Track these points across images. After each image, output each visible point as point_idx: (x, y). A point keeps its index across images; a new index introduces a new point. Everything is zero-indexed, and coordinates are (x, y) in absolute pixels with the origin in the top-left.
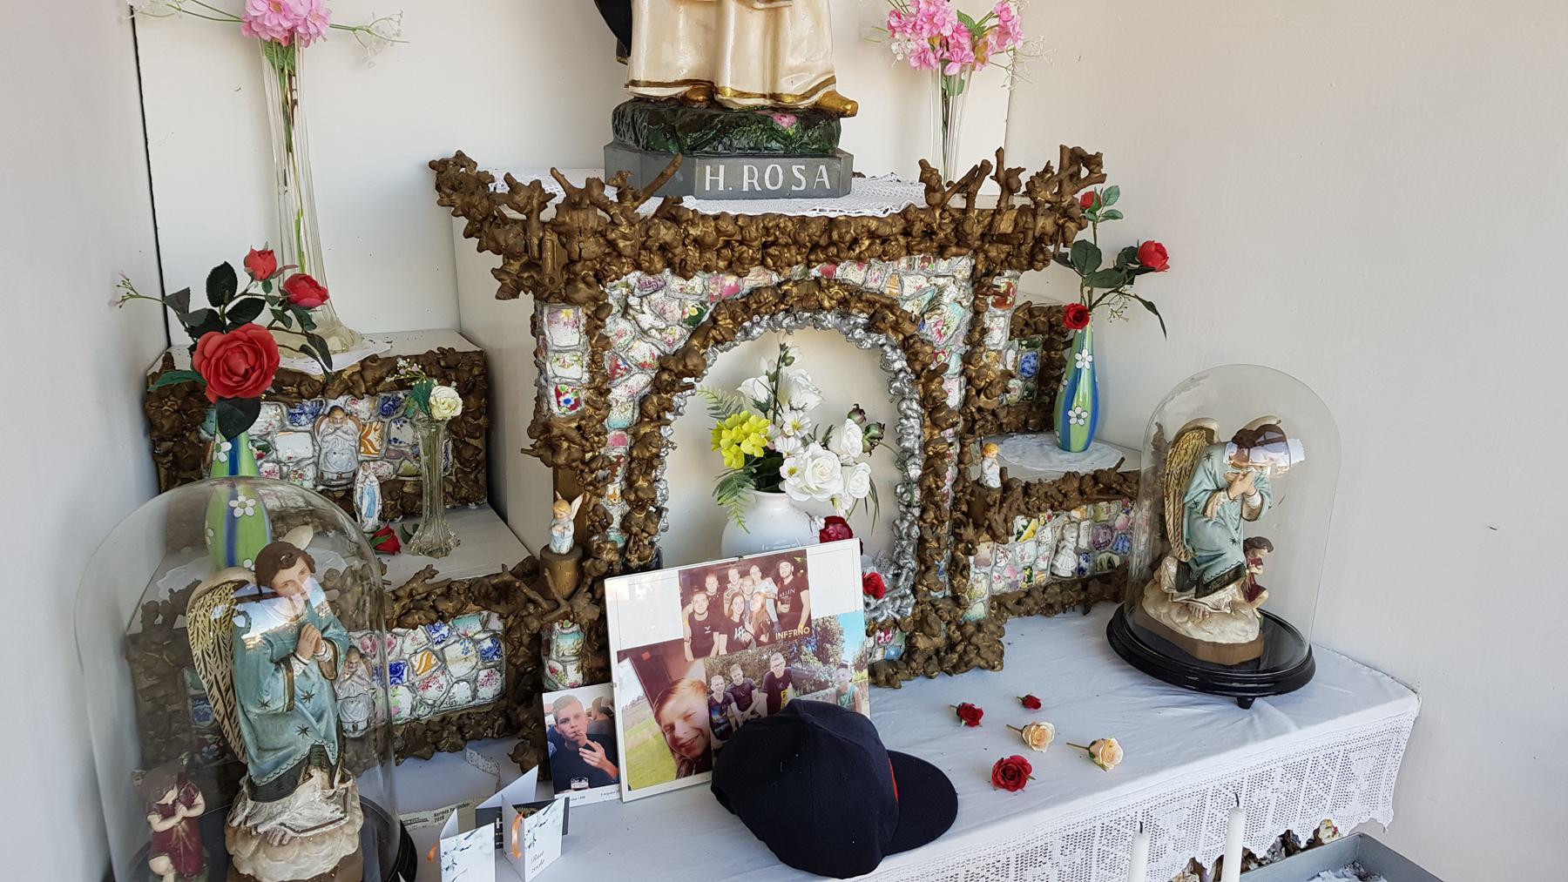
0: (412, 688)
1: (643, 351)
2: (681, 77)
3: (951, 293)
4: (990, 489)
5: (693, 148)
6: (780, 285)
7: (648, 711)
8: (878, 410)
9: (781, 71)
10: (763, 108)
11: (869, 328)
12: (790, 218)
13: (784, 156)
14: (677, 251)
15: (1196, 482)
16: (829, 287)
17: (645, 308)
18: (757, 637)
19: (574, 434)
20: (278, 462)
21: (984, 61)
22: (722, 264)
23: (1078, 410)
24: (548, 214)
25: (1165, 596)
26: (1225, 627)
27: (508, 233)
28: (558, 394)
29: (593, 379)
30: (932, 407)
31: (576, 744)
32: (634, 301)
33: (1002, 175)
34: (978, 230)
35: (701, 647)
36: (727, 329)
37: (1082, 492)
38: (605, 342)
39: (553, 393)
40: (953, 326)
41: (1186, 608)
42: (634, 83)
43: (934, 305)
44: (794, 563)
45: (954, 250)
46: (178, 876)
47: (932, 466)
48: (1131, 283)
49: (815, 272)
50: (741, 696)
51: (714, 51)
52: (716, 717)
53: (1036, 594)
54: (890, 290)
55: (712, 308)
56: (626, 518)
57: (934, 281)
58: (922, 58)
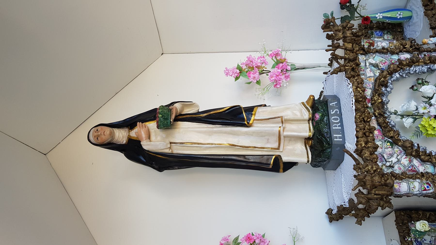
1: (405, 161)
2: (304, 148)
3: (371, 61)
5: (329, 144)
6: (376, 116)
8: (411, 81)
9: (302, 118)
10: (312, 123)
11: (386, 86)
12: (356, 114)
13: (329, 116)
14: (371, 150)
16: (375, 100)
21: (285, 59)
22: (371, 135)
23: (397, 15)
24: (365, 191)
27: (373, 205)
28: (425, 190)
29: (419, 178)
30: (412, 63)
32: (388, 164)
33: (334, 49)
34: (351, 54)
36: (394, 133)
38: (403, 173)
39: (425, 192)
40: (382, 59)
42: (308, 162)
43: (376, 66)
45: (357, 61)
49: (369, 105)
51: (295, 138)
55: (386, 138)
57: (367, 67)
58: (287, 77)
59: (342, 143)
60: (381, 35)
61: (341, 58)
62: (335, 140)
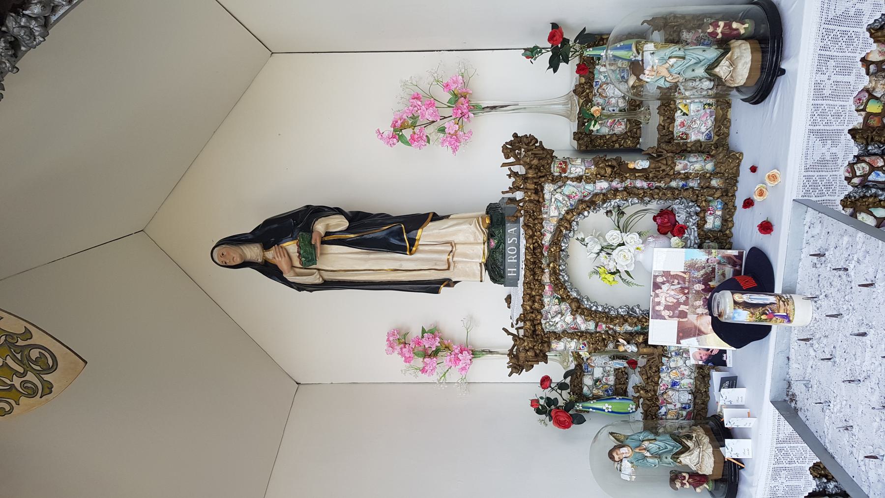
1: (569, 318)
18: (685, 294)
30: (605, 197)
35: (683, 314)
38: (564, 331)
46: (879, 204)
47: (630, 192)
54: (554, 222)
56: (630, 325)
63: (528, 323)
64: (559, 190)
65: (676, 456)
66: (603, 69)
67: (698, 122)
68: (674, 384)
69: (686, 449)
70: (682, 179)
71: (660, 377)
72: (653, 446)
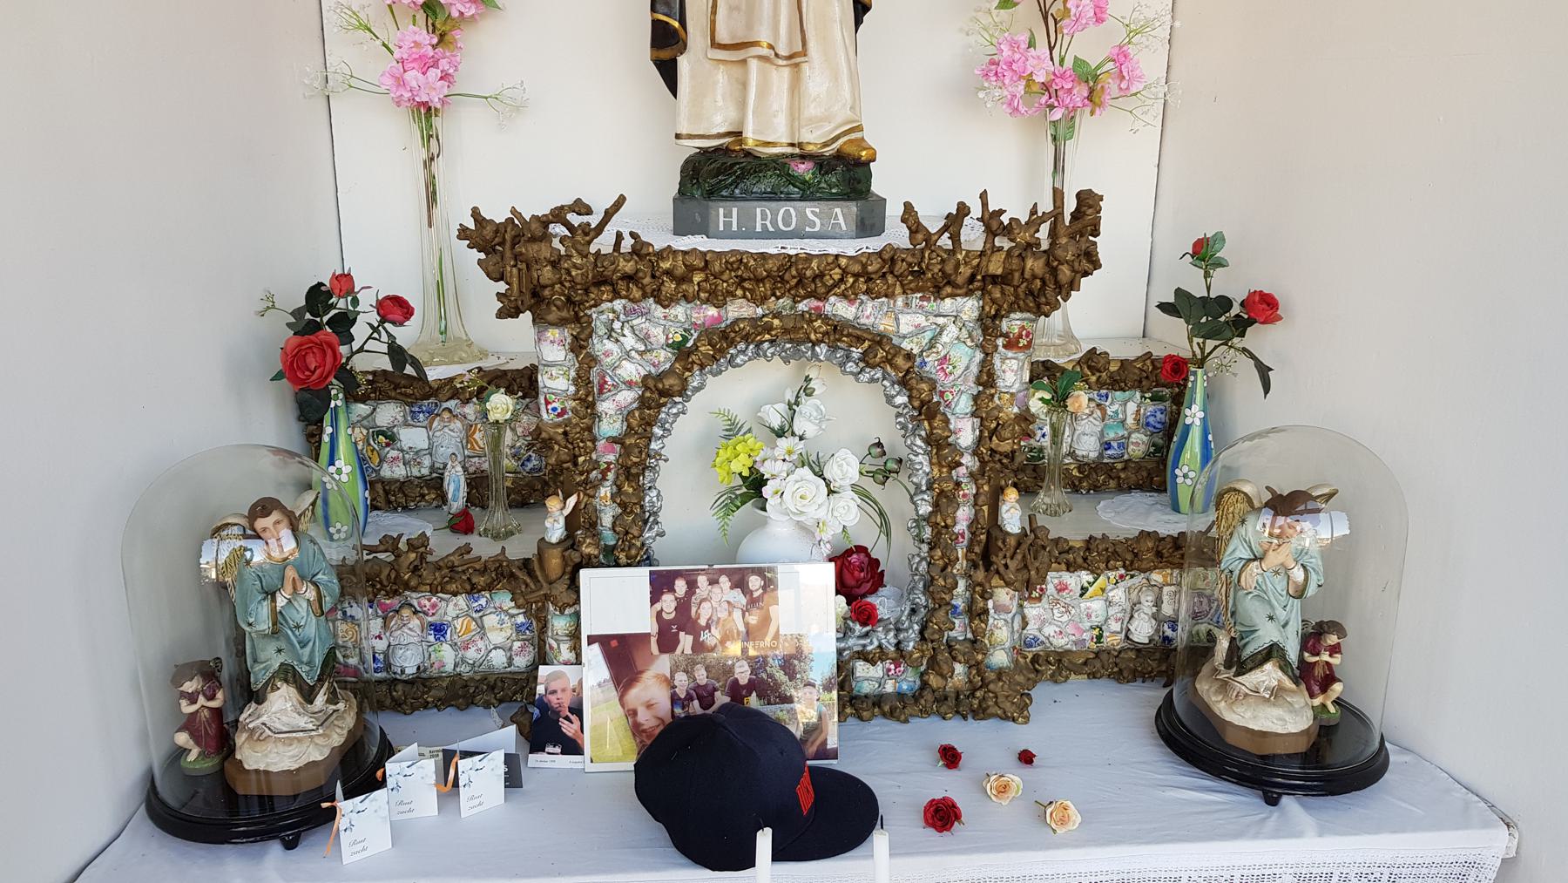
0: (454, 645)
1: (631, 370)
4: (1008, 534)
7: (613, 694)
15: (1230, 549)
17: (626, 332)
19: (560, 438)
20: (402, 451)
23: (1186, 469)
25: (1215, 671)
26: (1268, 711)
28: (547, 403)
30: (939, 445)
31: (558, 714)
32: (617, 325)
37: (1159, 554)
38: (593, 360)
39: (542, 401)
41: (1224, 687)
44: (764, 578)
47: (944, 500)
48: (1242, 335)
50: (704, 695)
52: (678, 711)
53: (1104, 656)
54: (884, 325)
59: (712, 230)
60: (1148, 424)
61: (955, 238)
62: (721, 211)
63: (629, 267)
64: (964, 334)
65: (288, 674)
66: (1132, 407)
67: (1065, 618)
68: (439, 629)
69: (308, 695)
70: (971, 604)
71: (455, 594)
72: (302, 613)
